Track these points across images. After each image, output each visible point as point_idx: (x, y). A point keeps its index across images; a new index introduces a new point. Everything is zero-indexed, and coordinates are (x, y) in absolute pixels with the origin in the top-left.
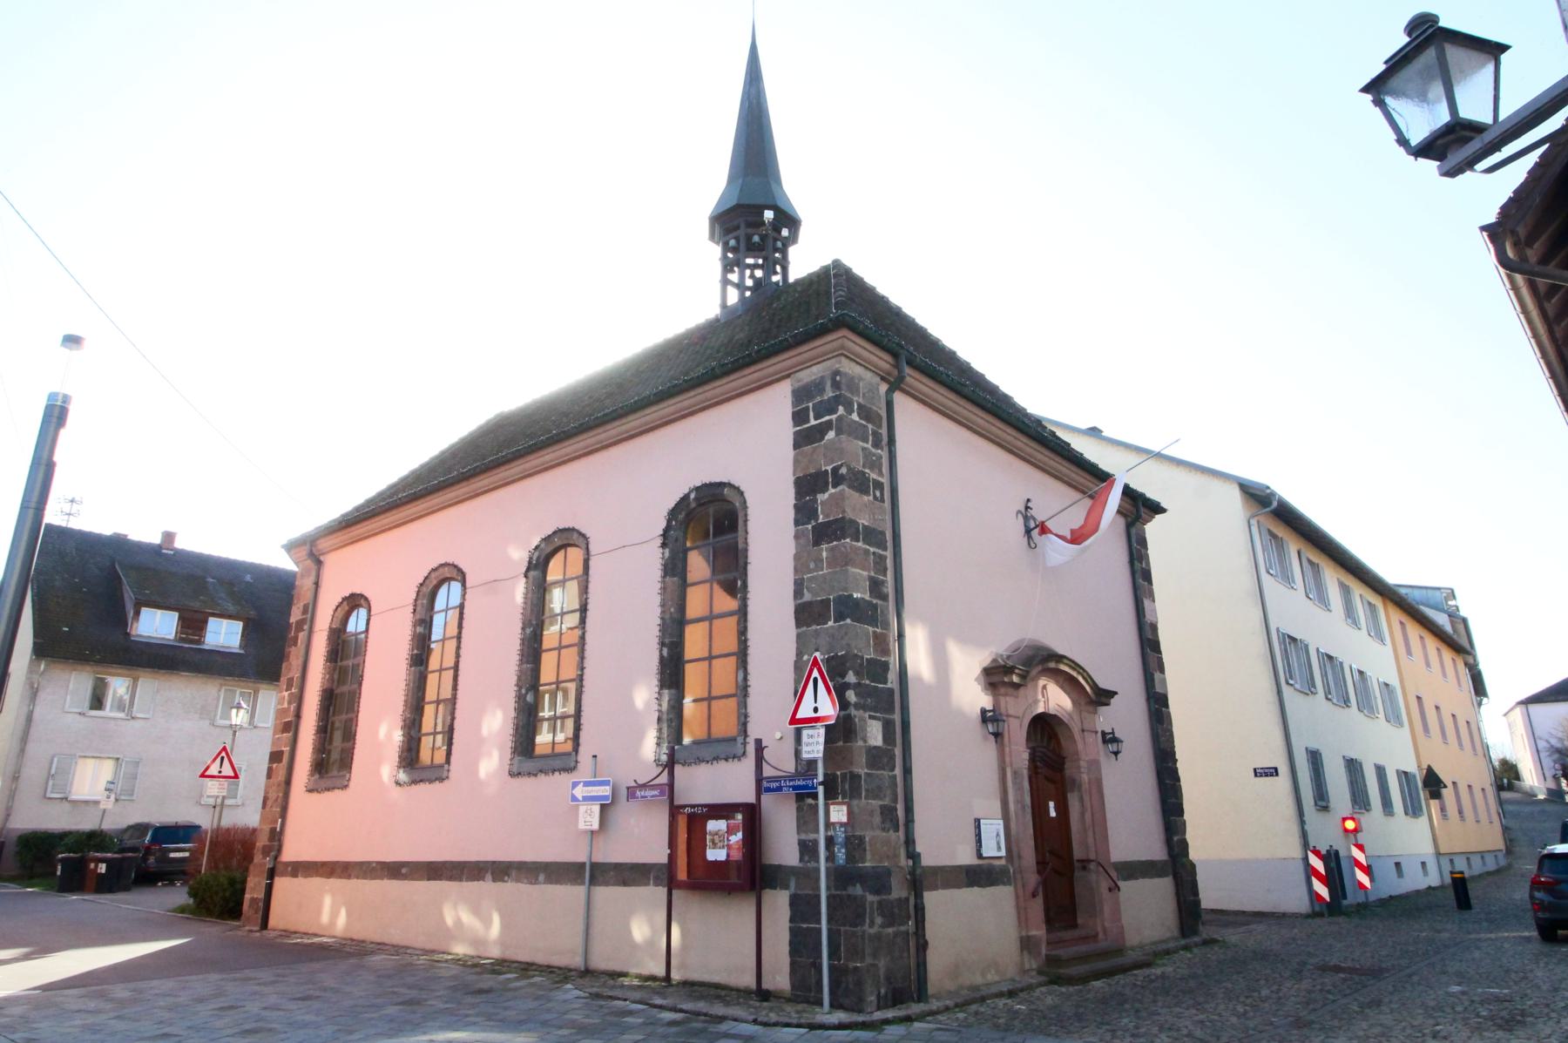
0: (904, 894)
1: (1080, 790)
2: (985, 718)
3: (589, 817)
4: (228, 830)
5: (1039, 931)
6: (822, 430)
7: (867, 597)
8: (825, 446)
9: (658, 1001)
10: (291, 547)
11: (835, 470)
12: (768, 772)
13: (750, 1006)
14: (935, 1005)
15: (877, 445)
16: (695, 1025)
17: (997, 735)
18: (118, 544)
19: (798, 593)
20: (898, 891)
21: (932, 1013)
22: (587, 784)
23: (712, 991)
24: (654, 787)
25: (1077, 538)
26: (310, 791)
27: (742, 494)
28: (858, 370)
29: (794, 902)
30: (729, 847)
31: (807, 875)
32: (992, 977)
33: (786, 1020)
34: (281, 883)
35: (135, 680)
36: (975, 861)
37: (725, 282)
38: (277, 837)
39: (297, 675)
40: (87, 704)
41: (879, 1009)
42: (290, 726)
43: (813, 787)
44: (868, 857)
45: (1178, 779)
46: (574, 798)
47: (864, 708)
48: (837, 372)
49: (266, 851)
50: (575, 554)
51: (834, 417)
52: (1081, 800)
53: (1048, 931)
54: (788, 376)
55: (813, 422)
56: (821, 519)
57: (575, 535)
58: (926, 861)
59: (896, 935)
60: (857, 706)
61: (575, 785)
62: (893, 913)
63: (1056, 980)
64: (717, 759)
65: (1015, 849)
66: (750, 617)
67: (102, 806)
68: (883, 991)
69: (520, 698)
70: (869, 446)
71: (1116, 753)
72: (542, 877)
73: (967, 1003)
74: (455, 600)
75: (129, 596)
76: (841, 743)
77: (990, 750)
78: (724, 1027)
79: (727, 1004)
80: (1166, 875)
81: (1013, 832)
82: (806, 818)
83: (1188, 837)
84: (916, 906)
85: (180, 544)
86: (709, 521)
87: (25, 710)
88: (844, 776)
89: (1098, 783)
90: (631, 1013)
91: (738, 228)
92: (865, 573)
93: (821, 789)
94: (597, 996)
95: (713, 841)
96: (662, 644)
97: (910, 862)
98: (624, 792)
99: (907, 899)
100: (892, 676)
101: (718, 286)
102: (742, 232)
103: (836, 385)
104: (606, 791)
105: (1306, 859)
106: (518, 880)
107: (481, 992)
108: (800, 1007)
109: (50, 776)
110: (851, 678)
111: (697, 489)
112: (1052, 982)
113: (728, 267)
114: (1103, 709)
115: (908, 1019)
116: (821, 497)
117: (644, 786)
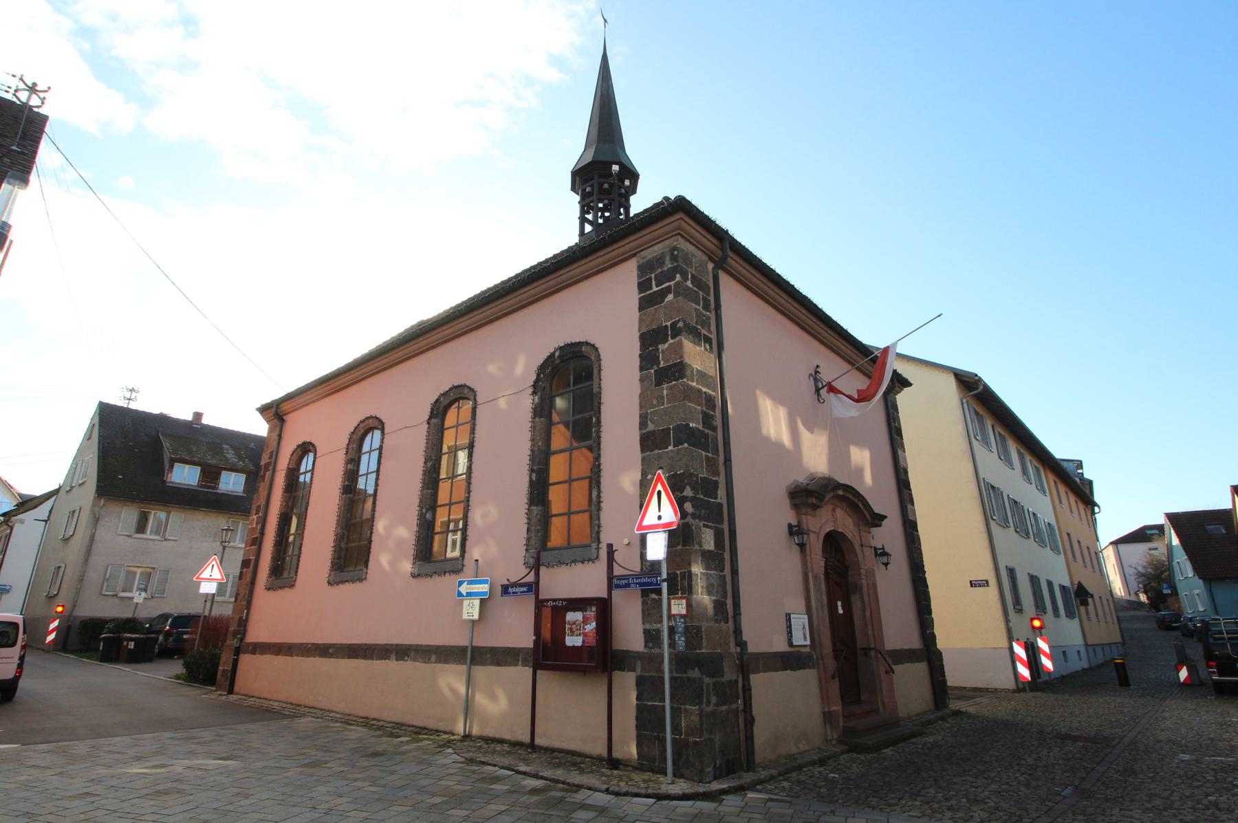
0: (734, 677)
3: (471, 610)
4: (215, 619)
5: (837, 708)
6: (663, 294)
7: (700, 427)
8: (665, 307)
9: (523, 768)
10: (264, 410)
11: (674, 325)
12: (618, 571)
13: (603, 775)
14: (763, 774)
15: (707, 307)
16: (554, 793)
17: (802, 546)
18: (162, 421)
19: (643, 425)
20: (729, 674)
21: (761, 782)
22: (470, 583)
23: (569, 758)
24: (522, 585)
26: (268, 589)
27: (597, 349)
28: (691, 248)
29: (640, 682)
30: (585, 635)
31: (653, 661)
32: (803, 747)
33: (636, 790)
34: (246, 660)
35: (168, 513)
37: (583, 220)
38: (243, 624)
39: (262, 502)
40: (133, 528)
41: (715, 778)
42: (256, 542)
43: (657, 584)
44: (705, 644)
45: (927, 586)
46: (460, 594)
47: (700, 518)
48: (675, 248)
49: (235, 633)
50: (467, 406)
51: (672, 283)
52: (862, 600)
54: (634, 255)
55: (655, 289)
56: (662, 364)
57: (466, 390)
58: (752, 648)
60: (694, 516)
61: (461, 583)
62: (726, 693)
64: (574, 561)
65: (816, 637)
66: (602, 446)
67: (135, 601)
69: (421, 516)
71: (886, 564)
72: (433, 658)
73: (789, 771)
74: (376, 444)
75: (167, 455)
76: (680, 547)
78: (580, 796)
79: (582, 771)
81: (815, 624)
82: (651, 610)
84: (744, 686)
85: (205, 421)
86: (570, 372)
87: (89, 533)
88: (683, 575)
90: (497, 779)
91: (592, 179)
93: (665, 585)
94: (471, 761)
95: (571, 629)
96: (532, 471)
97: (739, 649)
98: (499, 589)
100: (722, 492)
101: (577, 222)
102: (595, 182)
103: (674, 258)
104: (484, 588)
105: (1011, 648)
106: (415, 660)
107: (376, 754)
108: (646, 776)
109: (105, 579)
110: (688, 492)
111: (561, 348)
112: (850, 751)
113: (584, 212)
114: (874, 530)
115: (740, 789)
116: (661, 347)
117: (515, 585)
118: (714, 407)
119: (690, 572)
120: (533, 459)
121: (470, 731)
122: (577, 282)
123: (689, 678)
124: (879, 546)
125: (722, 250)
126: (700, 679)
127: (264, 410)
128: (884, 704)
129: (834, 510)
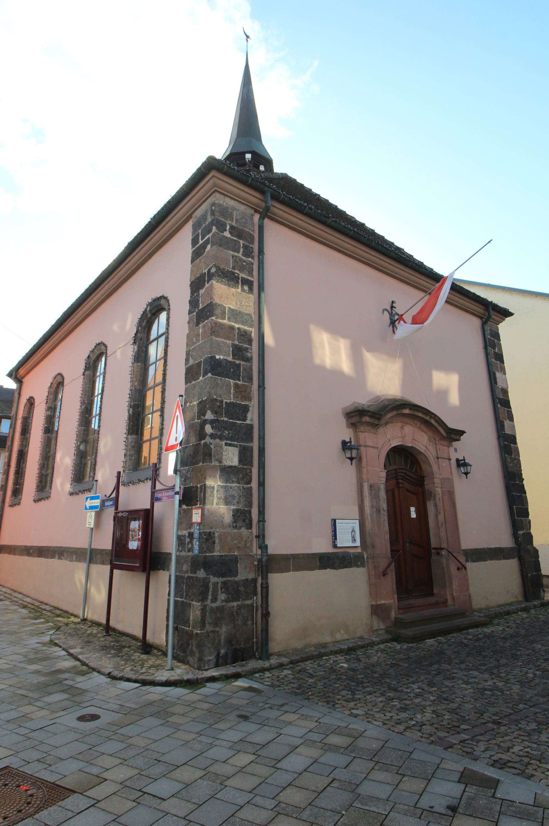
0: (251, 576)
1: (435, 499)
2: (345, 446)
5: (390, 600)
6: (204, 246)
7: (230, 359)
8: (205, 257)
10: (10, 375)
11: (209, 271)
14: (274, 661)
15: (248, 252)
19: (187, 360)
25: (418, 320)
28: (232, 203)
36: (331, 550)
45: (525, 492)
47: (221, 438)
52: (436, 506)
53: (399, 599)
59: (240, 607)
62: (235, 592)
63: (397, 639)
65: (368, 539)
68: (222, 651)
70: (240, 255)
71: (466, 474)
77: (349, 472)
80: (513, 558)
83: (533, 531)
88: (201, 486)
89: (451, 494)
92: (229, 342)
99: (255, 581)
118: (250, 341)
119: (205, 485)
120: (132, 397)
121: (87, 616)
122: (386, 274)
123: (197, 577)
124: (461, 458)
125: (266, 202)
126: (204, 579)
127: (10, 375)
128: (453, 599)
129: (402, 427)
